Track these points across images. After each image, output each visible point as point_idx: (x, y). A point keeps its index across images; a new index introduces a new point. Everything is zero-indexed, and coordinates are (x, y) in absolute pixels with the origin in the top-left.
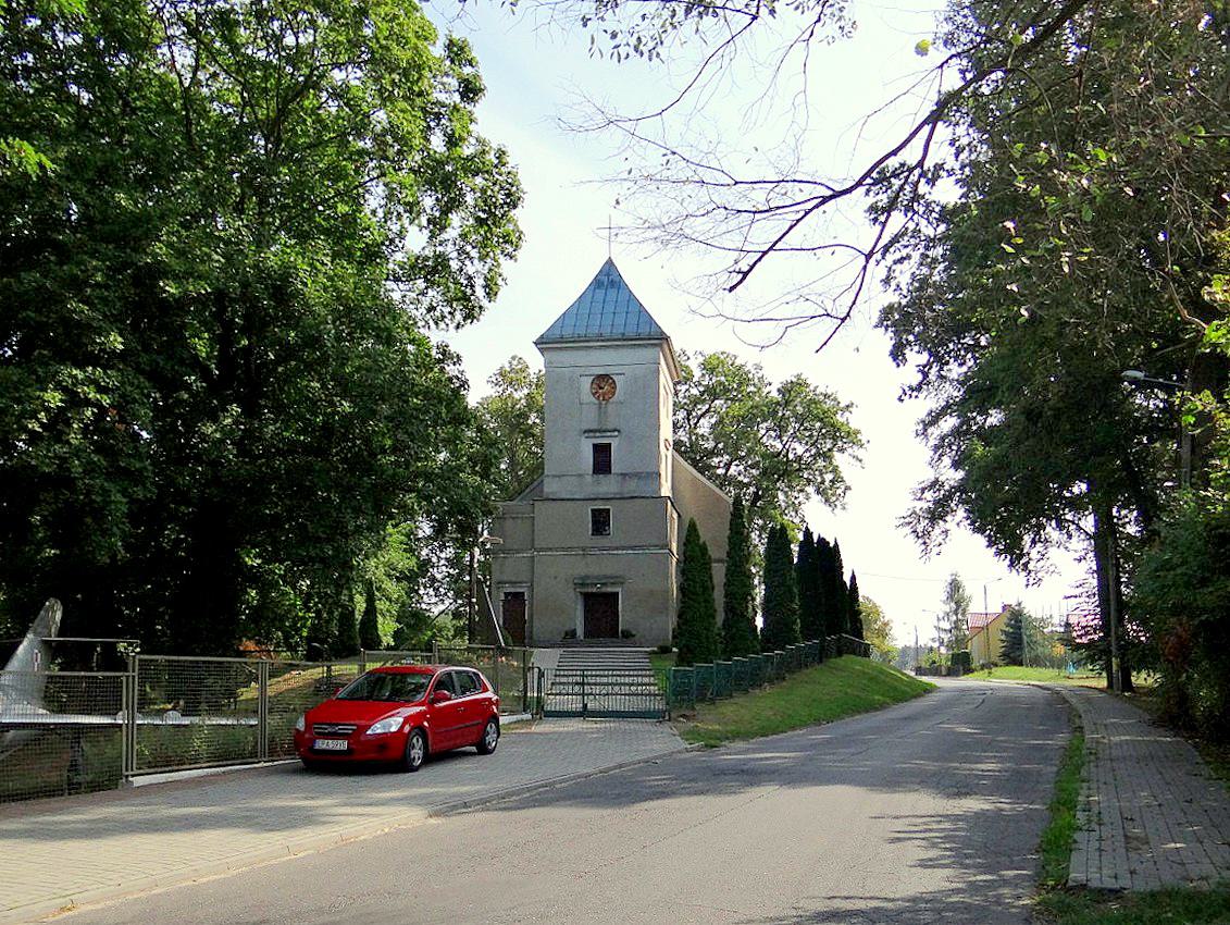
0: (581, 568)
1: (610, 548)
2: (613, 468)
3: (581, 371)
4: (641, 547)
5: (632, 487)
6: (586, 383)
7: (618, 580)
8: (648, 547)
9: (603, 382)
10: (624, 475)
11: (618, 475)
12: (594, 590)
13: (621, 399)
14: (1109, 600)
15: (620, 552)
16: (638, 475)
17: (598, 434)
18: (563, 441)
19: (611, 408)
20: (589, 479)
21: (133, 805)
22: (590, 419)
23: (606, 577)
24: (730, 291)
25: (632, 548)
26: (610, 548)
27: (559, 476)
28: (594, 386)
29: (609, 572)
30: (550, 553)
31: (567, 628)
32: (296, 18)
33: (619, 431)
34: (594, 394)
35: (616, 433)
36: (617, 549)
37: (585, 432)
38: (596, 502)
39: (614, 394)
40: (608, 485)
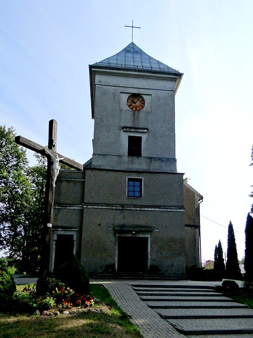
0: (120, 219)
1: (142, 206)
2: (142, 153)
3: (122, 89)
4: (164, 207)
5: (155, 166)
6: (125, 98)
7: (149, 230)
8: (170, 207)
9: (135, 98)
10: (150, 158)
11: (147, 158)
12: (130, 235)
13: (149, 110)
14: (176, 207)
15: (150, 209)
16: (160, 159)
17: (133, 130)
18: (108, 132)
19: (142, 115)
20: (126, 158)
21: (38, 148)
22: (127, 120)
23: (137, 226)
24: (151, 95)
25: (158, 207)
26: (142, 206)
27: (104, 155)
28: (130, 101)
29: (143, 223)
30: (96, 207)
31: (108, 263)
32: (3, 210)
33: (147, 129)
34: (129, 106)
35: (146, 131)
36: (147, 207)
37: (123, 128)
38: (131, 174)
39: (143, 107)
40: (139, 164)
